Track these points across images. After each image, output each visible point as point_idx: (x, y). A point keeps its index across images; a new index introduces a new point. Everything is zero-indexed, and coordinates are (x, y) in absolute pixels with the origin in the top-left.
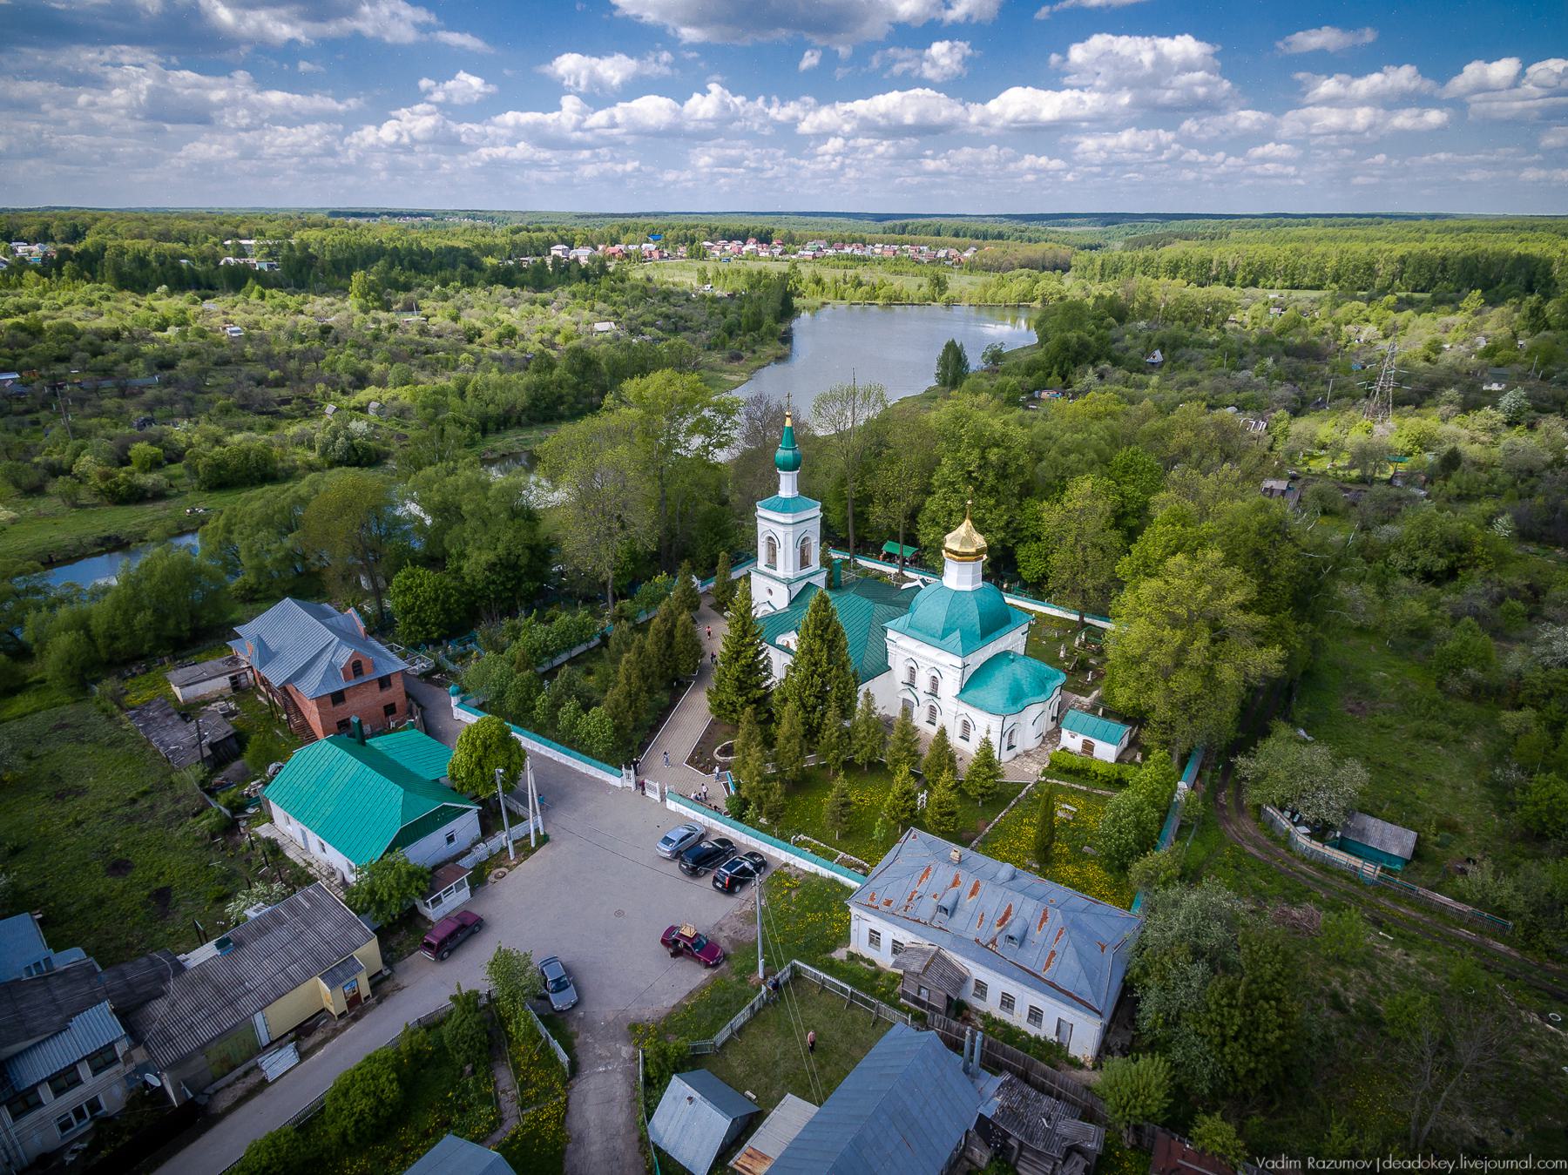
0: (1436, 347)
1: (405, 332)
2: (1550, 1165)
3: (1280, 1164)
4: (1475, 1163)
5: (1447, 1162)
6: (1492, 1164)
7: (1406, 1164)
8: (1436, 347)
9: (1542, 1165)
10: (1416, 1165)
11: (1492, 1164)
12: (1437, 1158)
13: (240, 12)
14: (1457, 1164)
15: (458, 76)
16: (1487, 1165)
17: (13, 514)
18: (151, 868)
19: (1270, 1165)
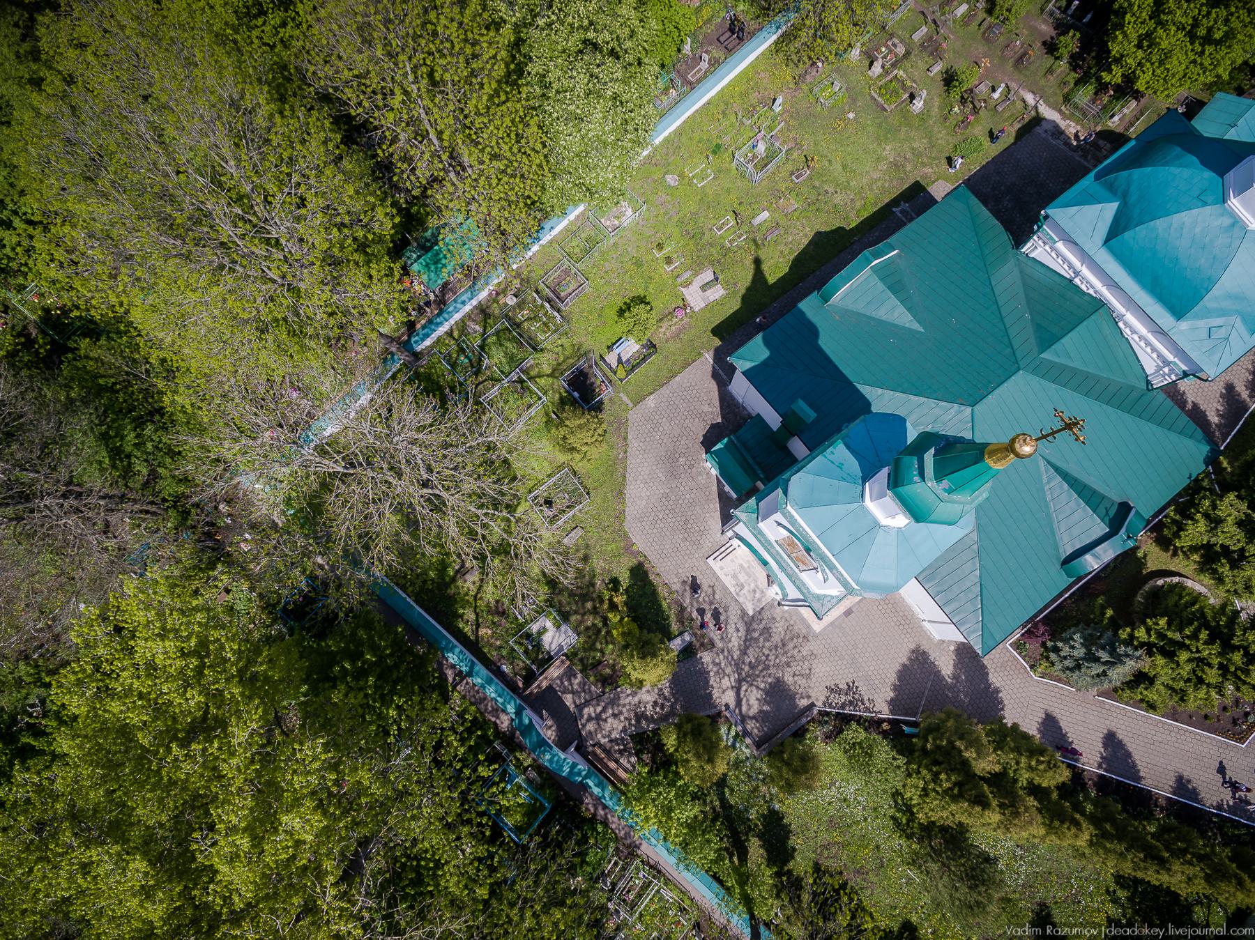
0: (757, 699)
1: (491, 534)
2: (1241, 932)
3: (1024, 932)
4: (1181, 930)
5: (1157, 930)
6: (1195, 932)
7: (1125, 932)
8: (757, 699)
9: (1234, 932)
10: (1133, 932)
11: (1195, 932)
12: (1150, 927)
13: (1106, 128)
14: (1167, 930)
15: (703, 305)
16: (1190, 932)
17: (885, 471)
18: (1231, 538)
19: (1017, 932)
